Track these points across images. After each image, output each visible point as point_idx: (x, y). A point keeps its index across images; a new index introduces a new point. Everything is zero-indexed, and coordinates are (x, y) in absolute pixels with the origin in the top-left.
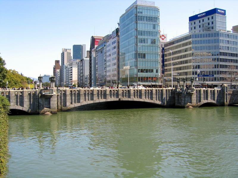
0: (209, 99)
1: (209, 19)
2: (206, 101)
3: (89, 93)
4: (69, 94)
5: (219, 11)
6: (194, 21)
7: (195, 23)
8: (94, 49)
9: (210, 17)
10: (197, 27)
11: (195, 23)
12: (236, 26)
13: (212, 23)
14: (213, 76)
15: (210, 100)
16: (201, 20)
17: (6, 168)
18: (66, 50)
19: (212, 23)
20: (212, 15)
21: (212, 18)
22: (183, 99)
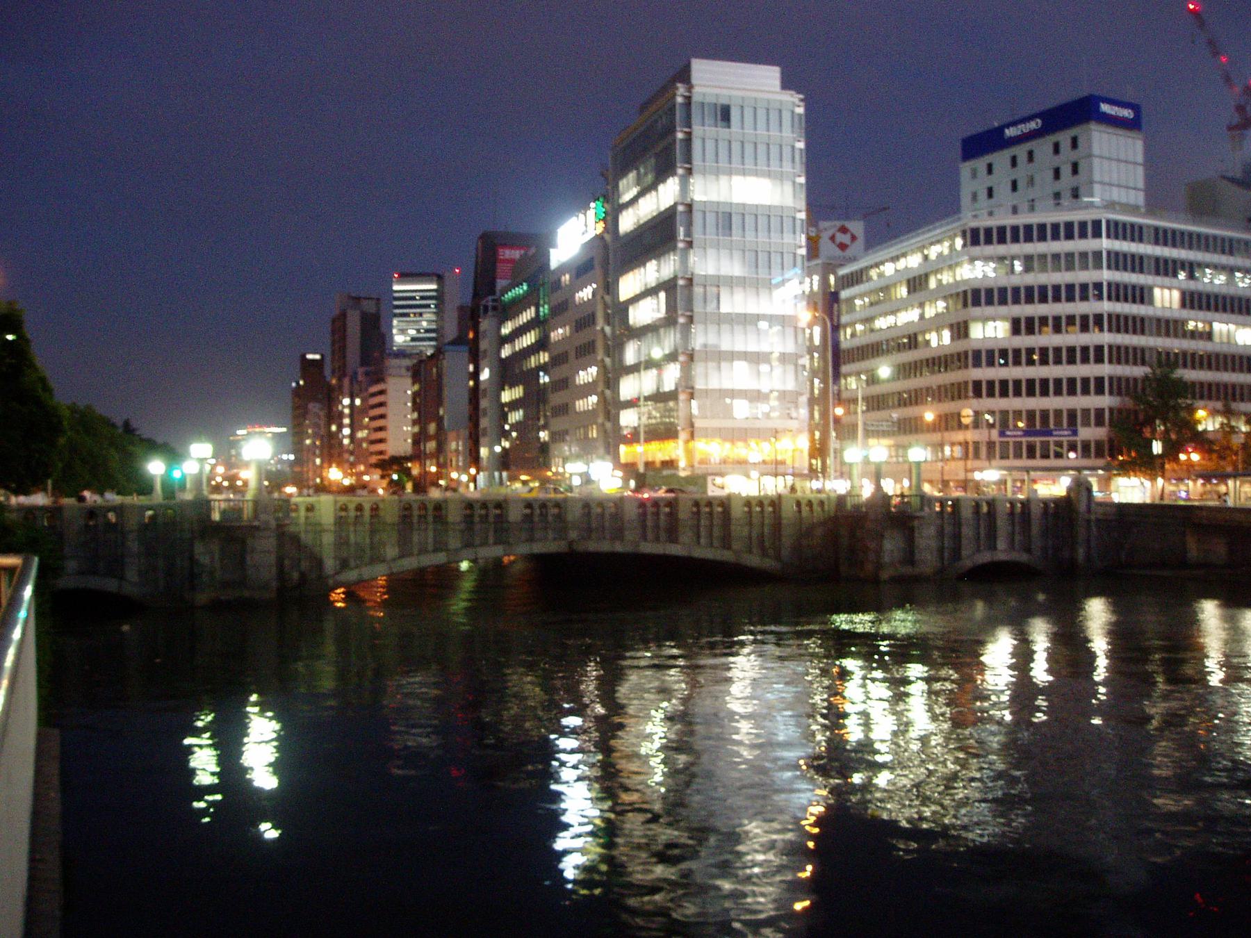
0: (1001, 544)
1: (1056, 149)
2: (985, 557)
3: (487, 515)
4: (458, 519)
5: (1105, 108)
6: (988, 159)
7: (990, 169)
8: (490, 298)
9: (1064, 137)
10: (1003, 191)
11: (990, 169)
12: (720, 59)
13: (1075, 169)
14: (1075, 433)
15: (1002, 552)
16: (1021, 151)
17: (724, 787)
18: (358, 299)
19: (1075, 169)
20: (1074, 131)
21: (1074, 143)
22: (872, 545)
